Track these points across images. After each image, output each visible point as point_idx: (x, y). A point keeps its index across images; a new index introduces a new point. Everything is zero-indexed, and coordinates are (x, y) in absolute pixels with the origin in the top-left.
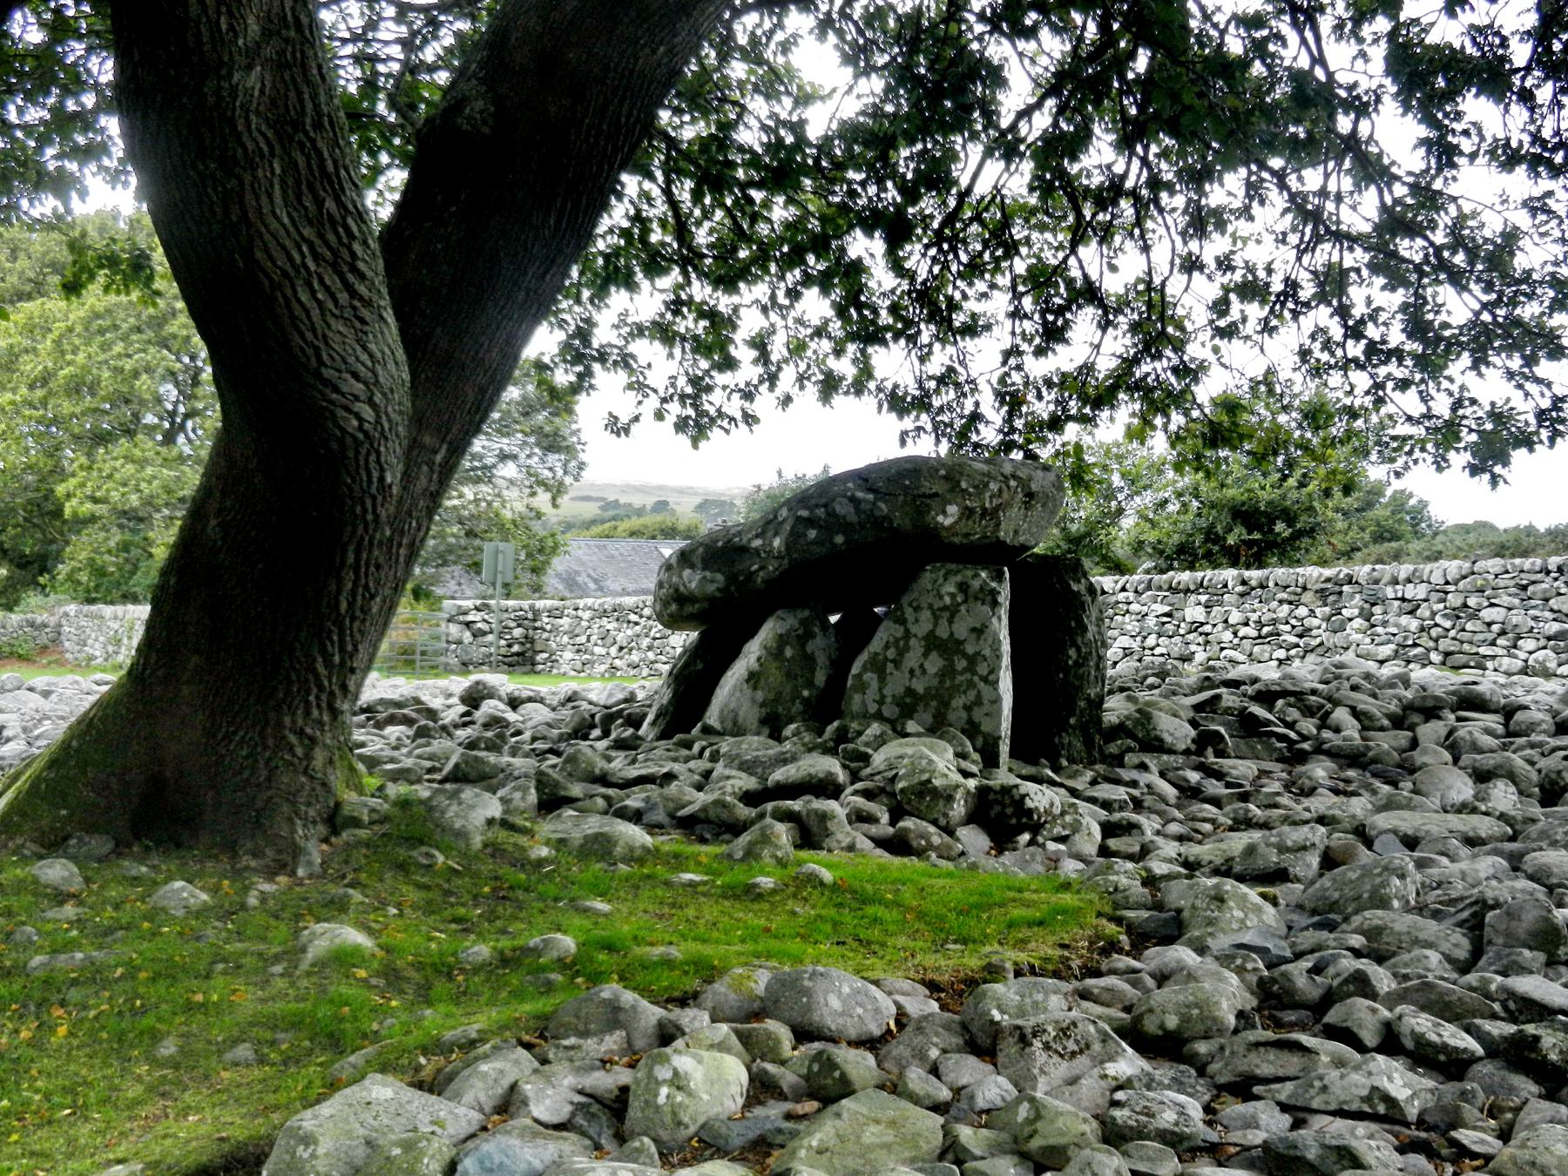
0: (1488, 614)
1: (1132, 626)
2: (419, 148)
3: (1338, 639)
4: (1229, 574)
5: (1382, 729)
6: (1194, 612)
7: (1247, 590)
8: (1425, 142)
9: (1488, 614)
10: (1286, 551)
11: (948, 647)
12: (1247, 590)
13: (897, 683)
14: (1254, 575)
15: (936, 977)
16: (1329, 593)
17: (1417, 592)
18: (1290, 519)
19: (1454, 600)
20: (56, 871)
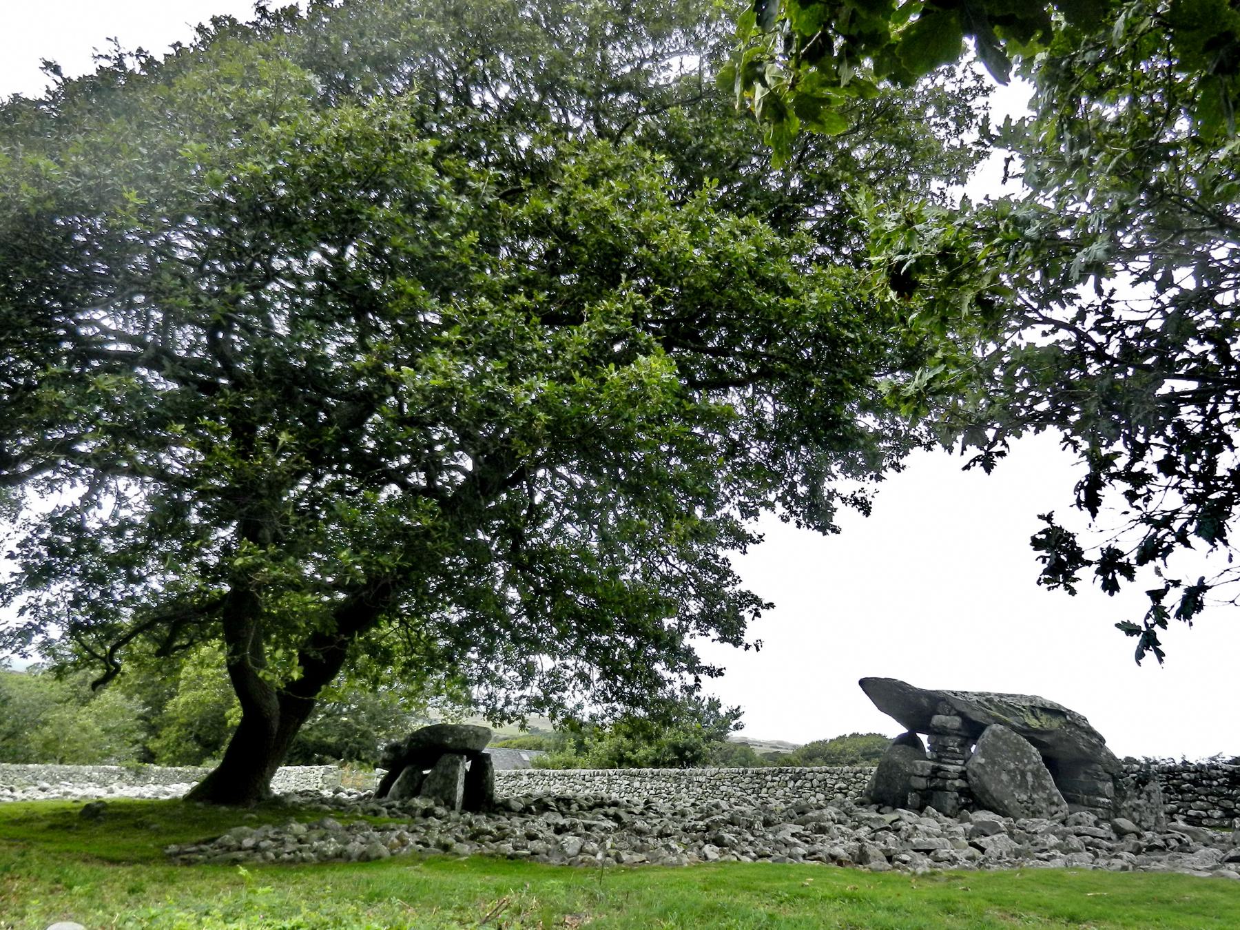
0: (722, 788)
1: (617, 789)
2: (3, 452)
3: (678, 796)
4: (648, 770)
5: (1077, 851)
6: (636, 784)
7: (653, 776)
8: (1075, 580)
9: (722, 788)
10: (692, 762)
11: (445, 776)
12: (653, 776)
13: (432, 787)
14: (656, 770)
15: (185, 870)
16: (677, 779)
17: (702, 779)
18: (692, 751)
19: (713, 782)
20: (199, 804)
